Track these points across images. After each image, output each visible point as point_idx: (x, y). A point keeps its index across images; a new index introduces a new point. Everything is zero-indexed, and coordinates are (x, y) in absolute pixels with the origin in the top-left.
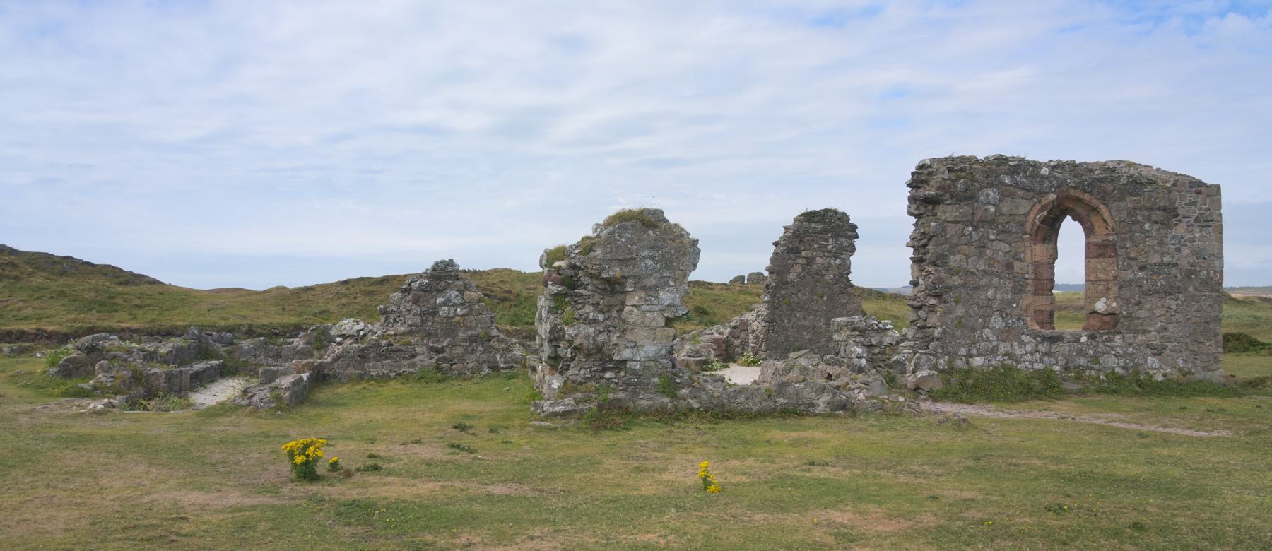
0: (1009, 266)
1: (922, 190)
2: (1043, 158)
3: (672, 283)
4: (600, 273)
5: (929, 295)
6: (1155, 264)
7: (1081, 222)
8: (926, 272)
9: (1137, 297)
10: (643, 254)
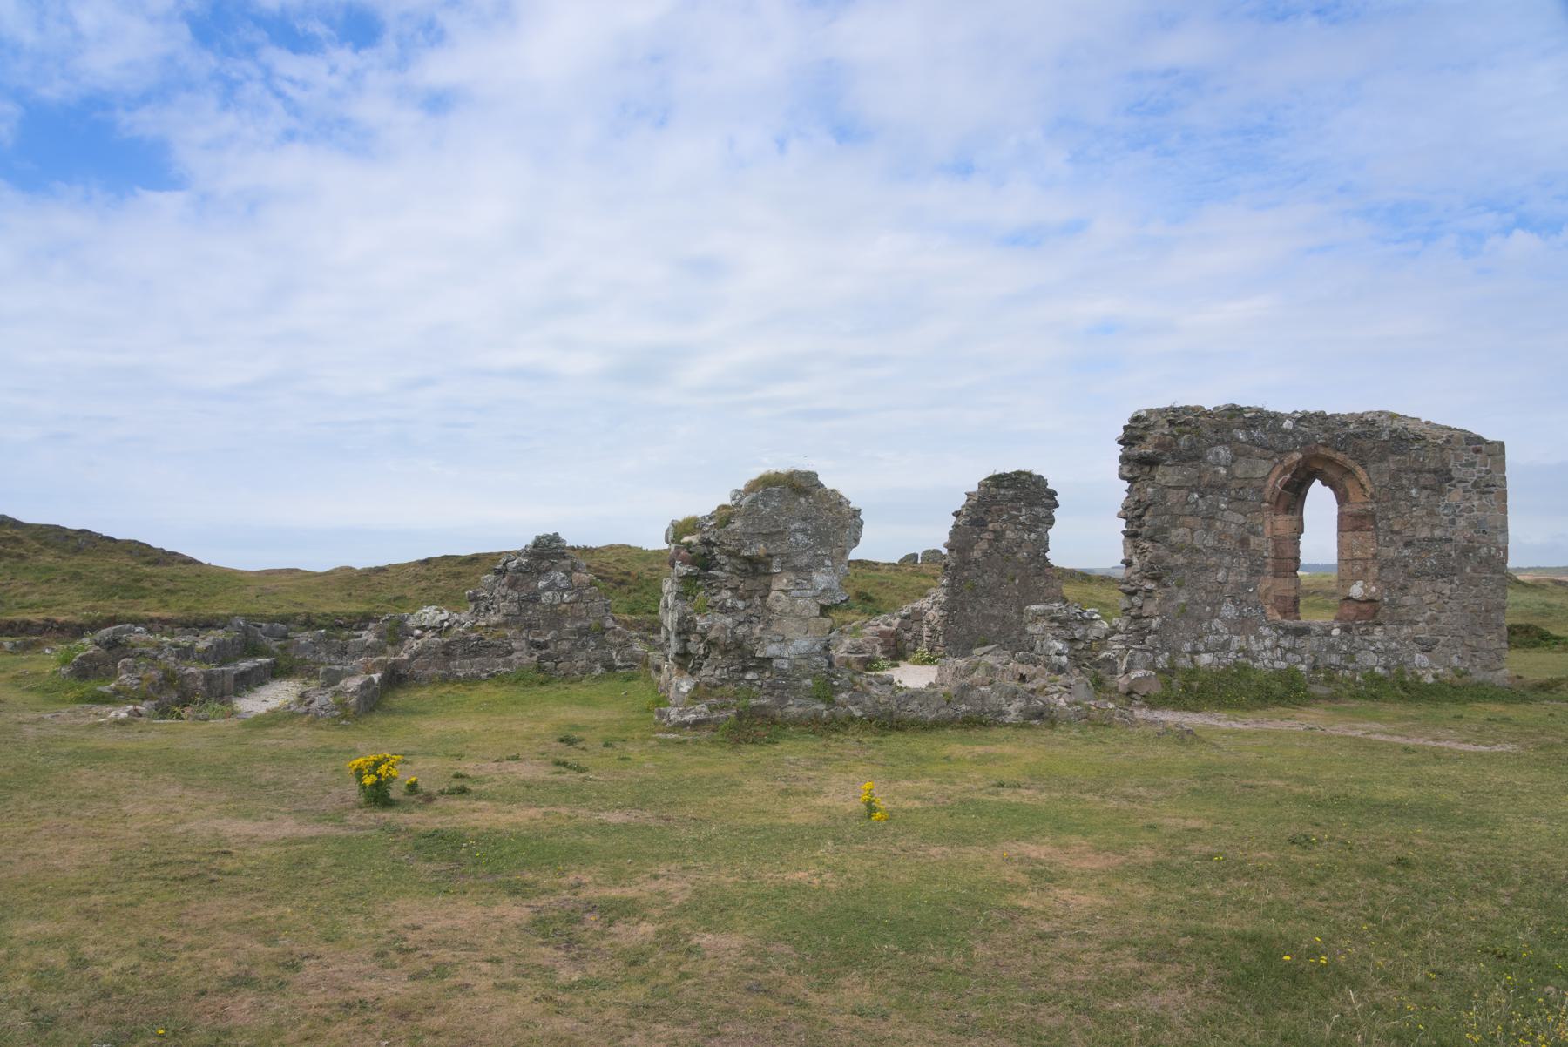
0: (1244, 542)
1: (1136, 447)
2: (1286, 409)
5: (1146, 577)
6: (1424, 540)
9: (1401, 580)
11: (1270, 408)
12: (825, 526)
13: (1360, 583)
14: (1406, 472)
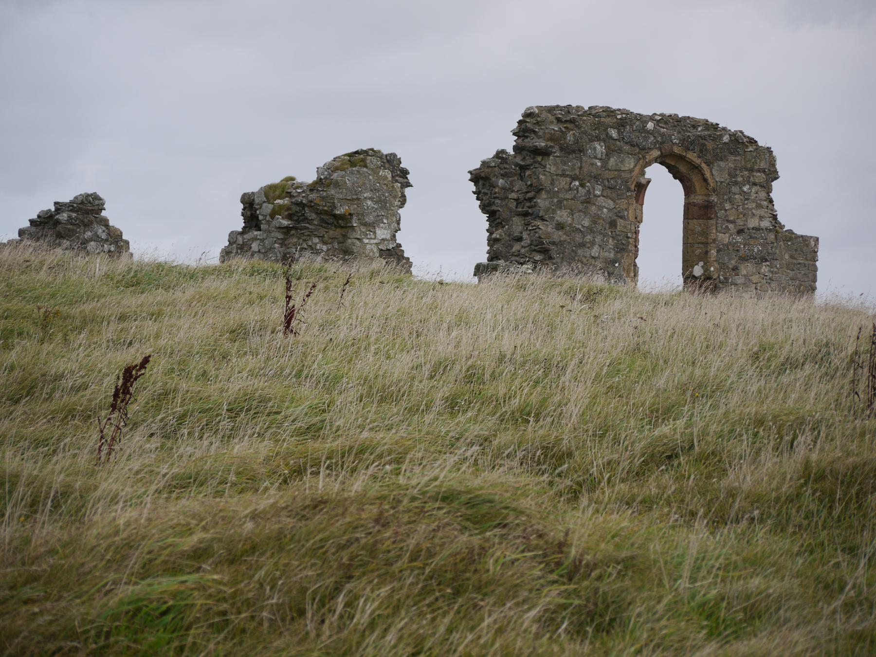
0: (613, 224)
1: (529, 139)
2: (647, 111)
3: (385, 221)
4: (332, 210)
5: (535, 250)
6: (753, 229)
7: (681, 181)
8: (532, 226)
9: (733, 262)
10: (365, 195)
11: (636, 110)
12: (384, 195)
13: (701, 264)
14: (741, 170)
